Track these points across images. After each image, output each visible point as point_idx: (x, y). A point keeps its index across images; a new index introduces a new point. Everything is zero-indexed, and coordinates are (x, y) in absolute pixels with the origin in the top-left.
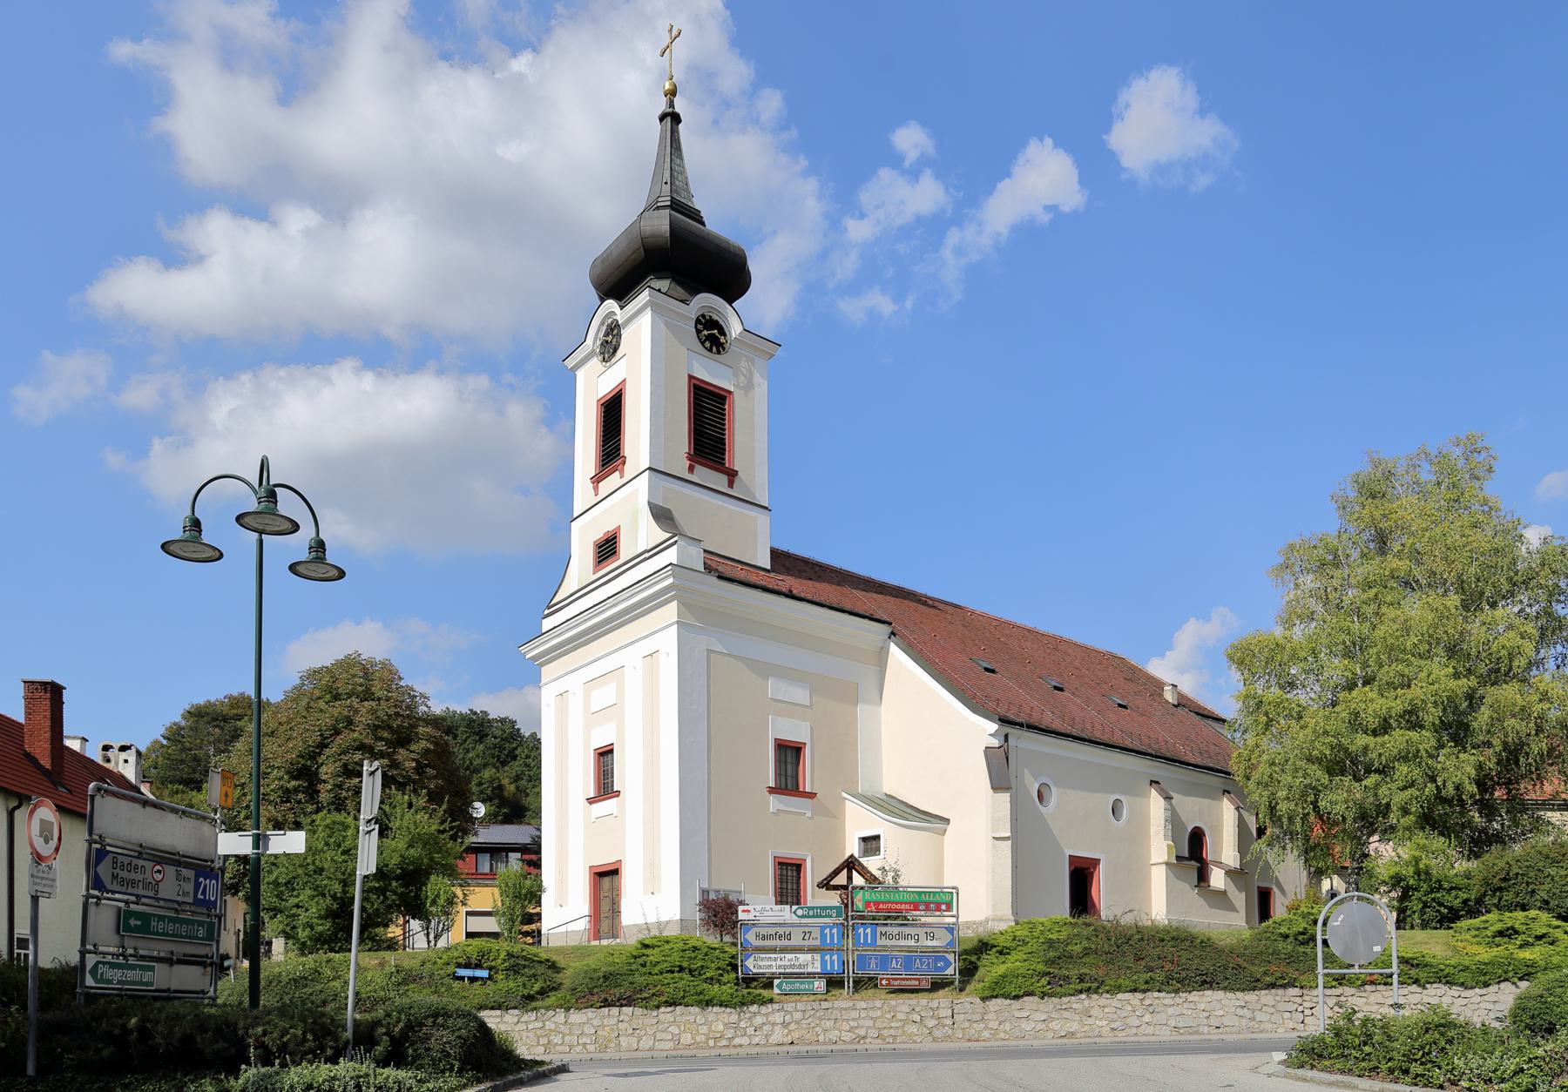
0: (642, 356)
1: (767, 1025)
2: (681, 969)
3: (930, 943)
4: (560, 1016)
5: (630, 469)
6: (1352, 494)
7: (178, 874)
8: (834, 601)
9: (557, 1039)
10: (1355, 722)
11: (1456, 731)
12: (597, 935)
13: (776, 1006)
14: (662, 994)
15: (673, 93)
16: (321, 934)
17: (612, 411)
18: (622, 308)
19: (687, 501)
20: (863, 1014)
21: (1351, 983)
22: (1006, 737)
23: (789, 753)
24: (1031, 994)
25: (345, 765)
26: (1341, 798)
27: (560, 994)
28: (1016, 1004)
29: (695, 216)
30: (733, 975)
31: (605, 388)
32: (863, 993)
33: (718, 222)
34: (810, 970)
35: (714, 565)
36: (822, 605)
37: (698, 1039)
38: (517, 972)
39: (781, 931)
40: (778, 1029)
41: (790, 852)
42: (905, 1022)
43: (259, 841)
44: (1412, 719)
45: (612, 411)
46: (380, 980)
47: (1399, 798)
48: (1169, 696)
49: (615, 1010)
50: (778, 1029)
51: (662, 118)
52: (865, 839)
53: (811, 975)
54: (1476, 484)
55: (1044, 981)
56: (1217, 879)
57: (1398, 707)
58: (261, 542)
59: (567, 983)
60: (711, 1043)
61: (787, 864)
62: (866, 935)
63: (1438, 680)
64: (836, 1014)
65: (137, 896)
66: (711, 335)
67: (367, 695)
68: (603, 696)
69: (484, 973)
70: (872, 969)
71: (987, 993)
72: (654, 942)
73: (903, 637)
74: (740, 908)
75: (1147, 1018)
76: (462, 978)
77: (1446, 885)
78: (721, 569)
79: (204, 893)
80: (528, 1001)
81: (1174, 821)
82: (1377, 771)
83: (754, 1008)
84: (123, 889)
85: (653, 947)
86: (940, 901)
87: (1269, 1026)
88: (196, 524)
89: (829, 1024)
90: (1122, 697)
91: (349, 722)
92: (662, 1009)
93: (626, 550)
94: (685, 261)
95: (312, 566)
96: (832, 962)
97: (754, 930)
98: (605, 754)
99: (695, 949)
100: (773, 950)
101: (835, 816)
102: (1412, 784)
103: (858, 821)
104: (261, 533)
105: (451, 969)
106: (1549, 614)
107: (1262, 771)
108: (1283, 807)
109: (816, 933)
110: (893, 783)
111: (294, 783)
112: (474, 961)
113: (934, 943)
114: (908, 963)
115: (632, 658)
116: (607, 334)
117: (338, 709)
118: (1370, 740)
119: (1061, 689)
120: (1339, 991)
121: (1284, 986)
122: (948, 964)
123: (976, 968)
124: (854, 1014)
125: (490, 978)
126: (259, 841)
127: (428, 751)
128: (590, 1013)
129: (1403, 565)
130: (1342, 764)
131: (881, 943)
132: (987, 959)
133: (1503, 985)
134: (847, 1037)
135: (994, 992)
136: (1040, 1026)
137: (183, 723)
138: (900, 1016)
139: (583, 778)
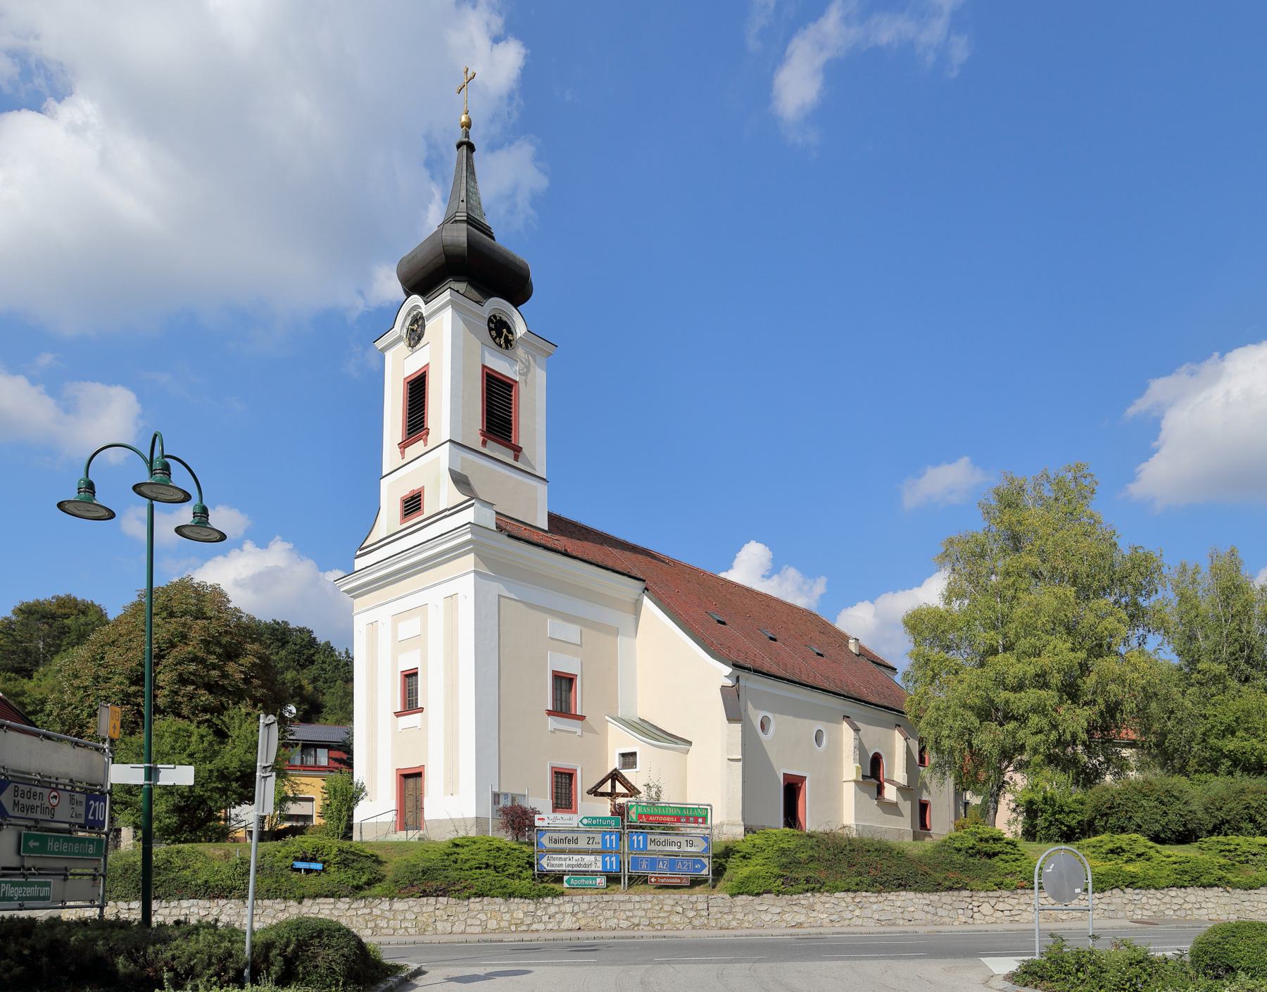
0: (443, 344)
1: (560, 917)
2: (488, 866)
3: (689, 849)
4: (386, 905)
5: (432, 439)
6: (994, 503)
7: (72, 798)
8: (599, 560)
9: (383, 924)
10: (1001, 682)
11: (1071, 692)
12: (403, 824)
13: (566, 899)
14: (472, 887)
15: (468, 125)
16: (168, 826)
17: (417, 389)
18: (426, 303)
19: (486, 472)
20: (637, 906)
21: (1007, 888)
22: (738, 678)
23: (564, 682)
24: (769, 892)
25: (180, 675)
26: (989, 738)
27: (385, 885)
28: (757, 900)
29: (487, 231)
30: (530, 872)
31: (412, 366)
32: (635, 887)
33: (509, 237)
34: (593, 868)
35: (503, 525)
36: (591, 563)
37: (502, 924)
38: (346, 866)
39: (570, 836)
40: (568, 917)
41: (565, 764)
42: (670, 913)
43: (151, 773)
44: (1041, 680)
45: (417, 389)
46: (226, 870)
47: (1031, 741)
48: (852, 647)
49: (432, 900)
50: (568, 917)
51: (459, 146)
52: (623, 755)
53: (594, 873)
54: (1085, 501)
55: (779, 882)
56: (890, 793)
57: (1031, 671)
58: (152, 507)
59: (390, 876)
60: (513, 928)
61: (562, 773)
62: (639, 842)
63: (1060, 653)
64: (615, 905)
65: (36, 821)
66: (499, 330)
67: (200, 615)
68: (410, 628)
69: (319, 866)
70: (643, 869)
71: (735, 891)
72: (463, 842)
73: (654, 592)
74: (537, 817)
75: (857, 912)
76: (299, 870)
77: (1066, 809)
78: (510, 528)
79: (94, 814)
80: (357, 891)
81: (860, 748)
82: (1016, 719)
83: (548, 900)
84: (24, 815)
85: (463, 846)
86: (698, 816)
87: (947, 920)
88: (90, 487)
89: (610, 914)
90: (819, 648)
91: (184, 637)
92: (472, 900)
93: (429, 507)
94: (476, 269)
95: (197, 530)
96: (611, 863)
97: (548, 834)
98: (410, 676)
99: (499, 849)
100: (562, 852)
101: (599, 733)
102: (1041, 732)
103: (618, 741)
104: (152, 500)
105: (289, 862)
106: (1136, 604)
107: (930, 715)
108: (946, 743)
109: (598, 838)
110: (645, 710)
111: (133, 688)
112: (309, 856)
113: (693, 849)
114: (672, 865)
115: (435, 598)
116: (412, 324)
117: (174, 625)
118: (1011, 696)
119: (774, 640)
120: (998, 893)
121: (959, 889)
122: (704, 866)
123: (725, 869)
124: (630, 906)
125: (324, 870)
126: (151, 773)
127: (254, 665)
128: (411, 902)
129: (1035, 561)
130: (986, 712)
131: (648, 848)
132: (733, 862)
133: (1115, 891)
134: (624, 924)
135: (742, 889)
136: (776, 918)
137: (14, 618)
138: (667, 908)
139: (391, 696)
